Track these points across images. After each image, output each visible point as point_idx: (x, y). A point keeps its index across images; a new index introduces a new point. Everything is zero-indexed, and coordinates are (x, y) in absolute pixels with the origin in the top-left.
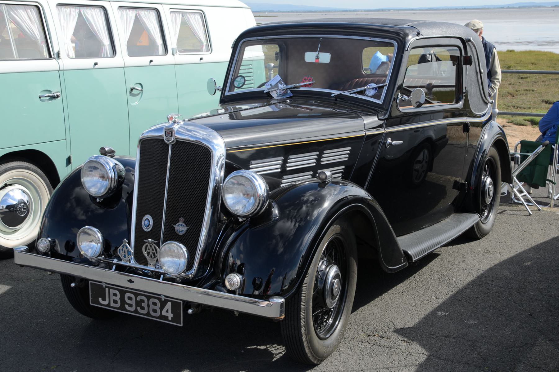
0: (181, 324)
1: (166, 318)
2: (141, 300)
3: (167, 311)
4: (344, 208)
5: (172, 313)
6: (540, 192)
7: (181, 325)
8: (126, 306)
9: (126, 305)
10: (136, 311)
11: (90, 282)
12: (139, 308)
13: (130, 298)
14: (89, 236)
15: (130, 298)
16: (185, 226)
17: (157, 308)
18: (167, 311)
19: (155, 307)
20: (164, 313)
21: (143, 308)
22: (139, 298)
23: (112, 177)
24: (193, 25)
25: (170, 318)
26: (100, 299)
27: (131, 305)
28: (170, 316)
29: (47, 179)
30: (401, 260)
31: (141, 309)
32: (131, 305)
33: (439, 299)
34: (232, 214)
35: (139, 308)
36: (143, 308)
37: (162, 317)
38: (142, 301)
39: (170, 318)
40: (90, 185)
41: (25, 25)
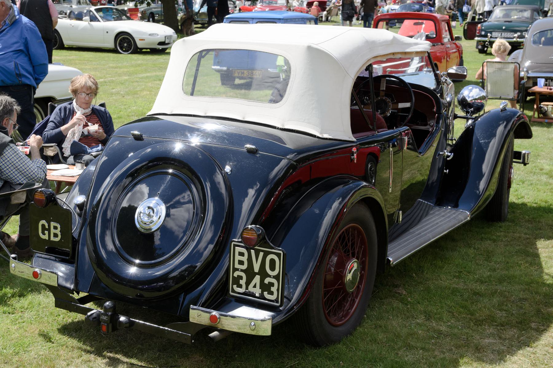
0: (234, 244)
1: (253, 295)
10: (262, 297)
12: (265, 293)
20: (251, 289)
21: (271, 293)
35: (265, 293)
36: (271, 293)
39: (257, 295)
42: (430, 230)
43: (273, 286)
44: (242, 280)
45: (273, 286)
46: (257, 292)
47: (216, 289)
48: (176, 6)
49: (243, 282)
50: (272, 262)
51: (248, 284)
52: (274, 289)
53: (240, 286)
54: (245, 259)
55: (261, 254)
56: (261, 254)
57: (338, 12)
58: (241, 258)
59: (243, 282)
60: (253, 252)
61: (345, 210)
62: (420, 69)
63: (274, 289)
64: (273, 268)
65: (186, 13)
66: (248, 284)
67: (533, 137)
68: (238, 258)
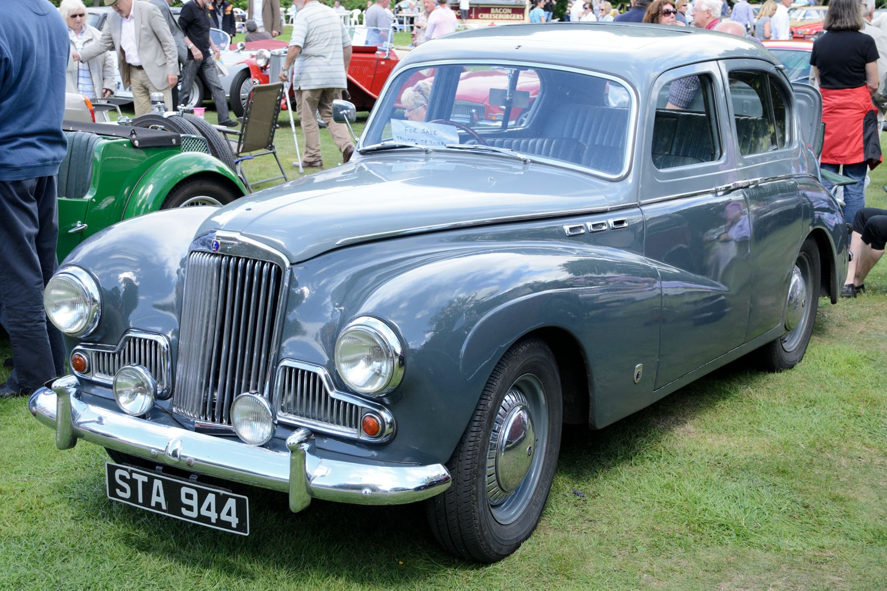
1: (228, 525)
5: (237, 517)
7: (247, 535)
8: (184, 510)
9: (182, 508)
13: (189, 496)
14: (483, 571)
15: (189, 496)
17: (194, 503)
20: (204, 512)
23: (307, 68)
24: (803, 333)
25: (234, 525)
27: (190, 508)
28: (234, 520)
31: (121, 491)
32: (190, 508)
33: (720, 526)
34: (565, 427)
39: (234, 525)
41: (608, 255)
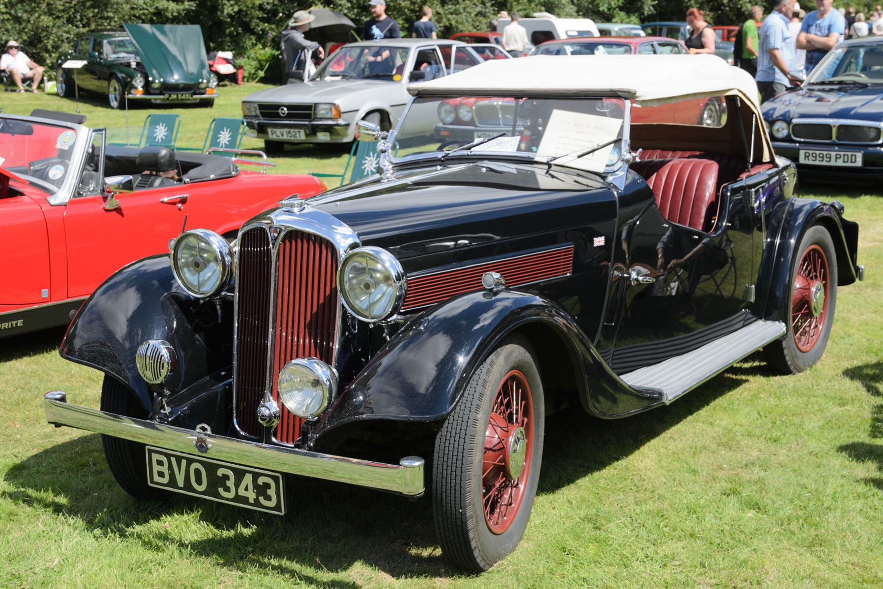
0: (148, 449)
1: (245, 500)
2: (264, 483)
3: (246, 489)
4: (691, 256)
6: (385, 133)
10: (257, 503)
11: (147, 447)
12: (261, 499)
16: (735, 365)
18: (246, 489)
19: (160, 468)
20: (242, 492)
21: (269, 498)
22: (261, 481)
25: (251, 501)
26: (221, 490)
29: (655, 124)
30: (385, 338)
31: (265, 499)
35: (261, 499)
36: (269, 498)
37: (238, 498)
38: (226, 477)
39: (251, 501)
40: (142, 84)
42: (732, 346)
43: (270, 488)
44: (229, 480)
45: (270, 488)
46: (251, 495)
47: (705, 361)
48: (219, 13)
49: (230, 483)
50: (197, 472)
51: (237, 486)
52: (272, 492)
53: (227, 489)
54: (165, 469)
55: (184, 462)
56: (184, 462)
57: (49, 94)
58: (160, 468)
59: (230, 483)
60: (173, 460)
61: (353, 386)
62: (701, 120)
63: (272, 492)
64: (199, 481)
65: (373, 10)
66: (237, 486)
67: (858, 223)
68: (156, 468)
